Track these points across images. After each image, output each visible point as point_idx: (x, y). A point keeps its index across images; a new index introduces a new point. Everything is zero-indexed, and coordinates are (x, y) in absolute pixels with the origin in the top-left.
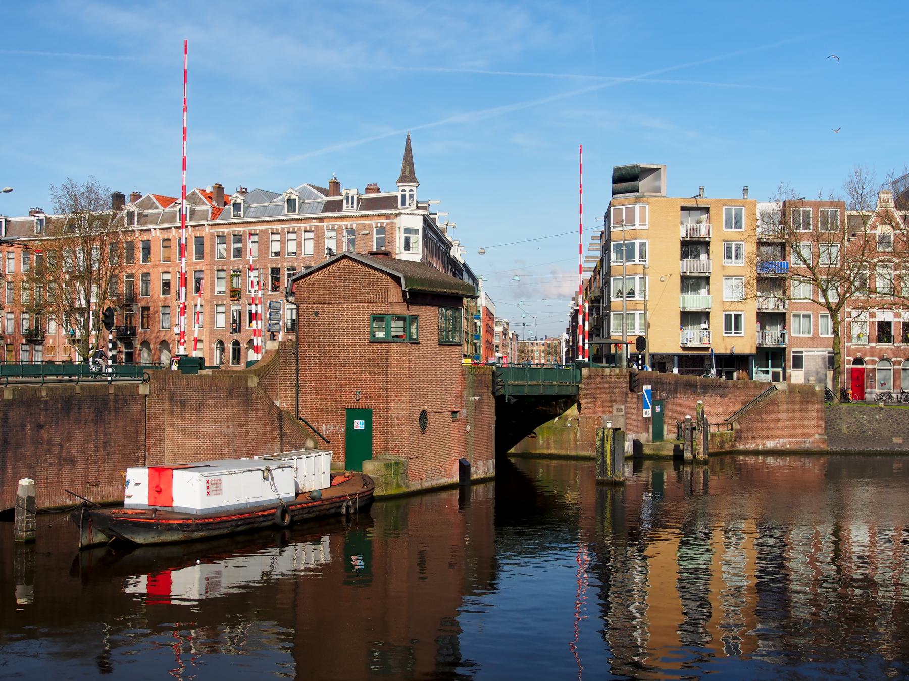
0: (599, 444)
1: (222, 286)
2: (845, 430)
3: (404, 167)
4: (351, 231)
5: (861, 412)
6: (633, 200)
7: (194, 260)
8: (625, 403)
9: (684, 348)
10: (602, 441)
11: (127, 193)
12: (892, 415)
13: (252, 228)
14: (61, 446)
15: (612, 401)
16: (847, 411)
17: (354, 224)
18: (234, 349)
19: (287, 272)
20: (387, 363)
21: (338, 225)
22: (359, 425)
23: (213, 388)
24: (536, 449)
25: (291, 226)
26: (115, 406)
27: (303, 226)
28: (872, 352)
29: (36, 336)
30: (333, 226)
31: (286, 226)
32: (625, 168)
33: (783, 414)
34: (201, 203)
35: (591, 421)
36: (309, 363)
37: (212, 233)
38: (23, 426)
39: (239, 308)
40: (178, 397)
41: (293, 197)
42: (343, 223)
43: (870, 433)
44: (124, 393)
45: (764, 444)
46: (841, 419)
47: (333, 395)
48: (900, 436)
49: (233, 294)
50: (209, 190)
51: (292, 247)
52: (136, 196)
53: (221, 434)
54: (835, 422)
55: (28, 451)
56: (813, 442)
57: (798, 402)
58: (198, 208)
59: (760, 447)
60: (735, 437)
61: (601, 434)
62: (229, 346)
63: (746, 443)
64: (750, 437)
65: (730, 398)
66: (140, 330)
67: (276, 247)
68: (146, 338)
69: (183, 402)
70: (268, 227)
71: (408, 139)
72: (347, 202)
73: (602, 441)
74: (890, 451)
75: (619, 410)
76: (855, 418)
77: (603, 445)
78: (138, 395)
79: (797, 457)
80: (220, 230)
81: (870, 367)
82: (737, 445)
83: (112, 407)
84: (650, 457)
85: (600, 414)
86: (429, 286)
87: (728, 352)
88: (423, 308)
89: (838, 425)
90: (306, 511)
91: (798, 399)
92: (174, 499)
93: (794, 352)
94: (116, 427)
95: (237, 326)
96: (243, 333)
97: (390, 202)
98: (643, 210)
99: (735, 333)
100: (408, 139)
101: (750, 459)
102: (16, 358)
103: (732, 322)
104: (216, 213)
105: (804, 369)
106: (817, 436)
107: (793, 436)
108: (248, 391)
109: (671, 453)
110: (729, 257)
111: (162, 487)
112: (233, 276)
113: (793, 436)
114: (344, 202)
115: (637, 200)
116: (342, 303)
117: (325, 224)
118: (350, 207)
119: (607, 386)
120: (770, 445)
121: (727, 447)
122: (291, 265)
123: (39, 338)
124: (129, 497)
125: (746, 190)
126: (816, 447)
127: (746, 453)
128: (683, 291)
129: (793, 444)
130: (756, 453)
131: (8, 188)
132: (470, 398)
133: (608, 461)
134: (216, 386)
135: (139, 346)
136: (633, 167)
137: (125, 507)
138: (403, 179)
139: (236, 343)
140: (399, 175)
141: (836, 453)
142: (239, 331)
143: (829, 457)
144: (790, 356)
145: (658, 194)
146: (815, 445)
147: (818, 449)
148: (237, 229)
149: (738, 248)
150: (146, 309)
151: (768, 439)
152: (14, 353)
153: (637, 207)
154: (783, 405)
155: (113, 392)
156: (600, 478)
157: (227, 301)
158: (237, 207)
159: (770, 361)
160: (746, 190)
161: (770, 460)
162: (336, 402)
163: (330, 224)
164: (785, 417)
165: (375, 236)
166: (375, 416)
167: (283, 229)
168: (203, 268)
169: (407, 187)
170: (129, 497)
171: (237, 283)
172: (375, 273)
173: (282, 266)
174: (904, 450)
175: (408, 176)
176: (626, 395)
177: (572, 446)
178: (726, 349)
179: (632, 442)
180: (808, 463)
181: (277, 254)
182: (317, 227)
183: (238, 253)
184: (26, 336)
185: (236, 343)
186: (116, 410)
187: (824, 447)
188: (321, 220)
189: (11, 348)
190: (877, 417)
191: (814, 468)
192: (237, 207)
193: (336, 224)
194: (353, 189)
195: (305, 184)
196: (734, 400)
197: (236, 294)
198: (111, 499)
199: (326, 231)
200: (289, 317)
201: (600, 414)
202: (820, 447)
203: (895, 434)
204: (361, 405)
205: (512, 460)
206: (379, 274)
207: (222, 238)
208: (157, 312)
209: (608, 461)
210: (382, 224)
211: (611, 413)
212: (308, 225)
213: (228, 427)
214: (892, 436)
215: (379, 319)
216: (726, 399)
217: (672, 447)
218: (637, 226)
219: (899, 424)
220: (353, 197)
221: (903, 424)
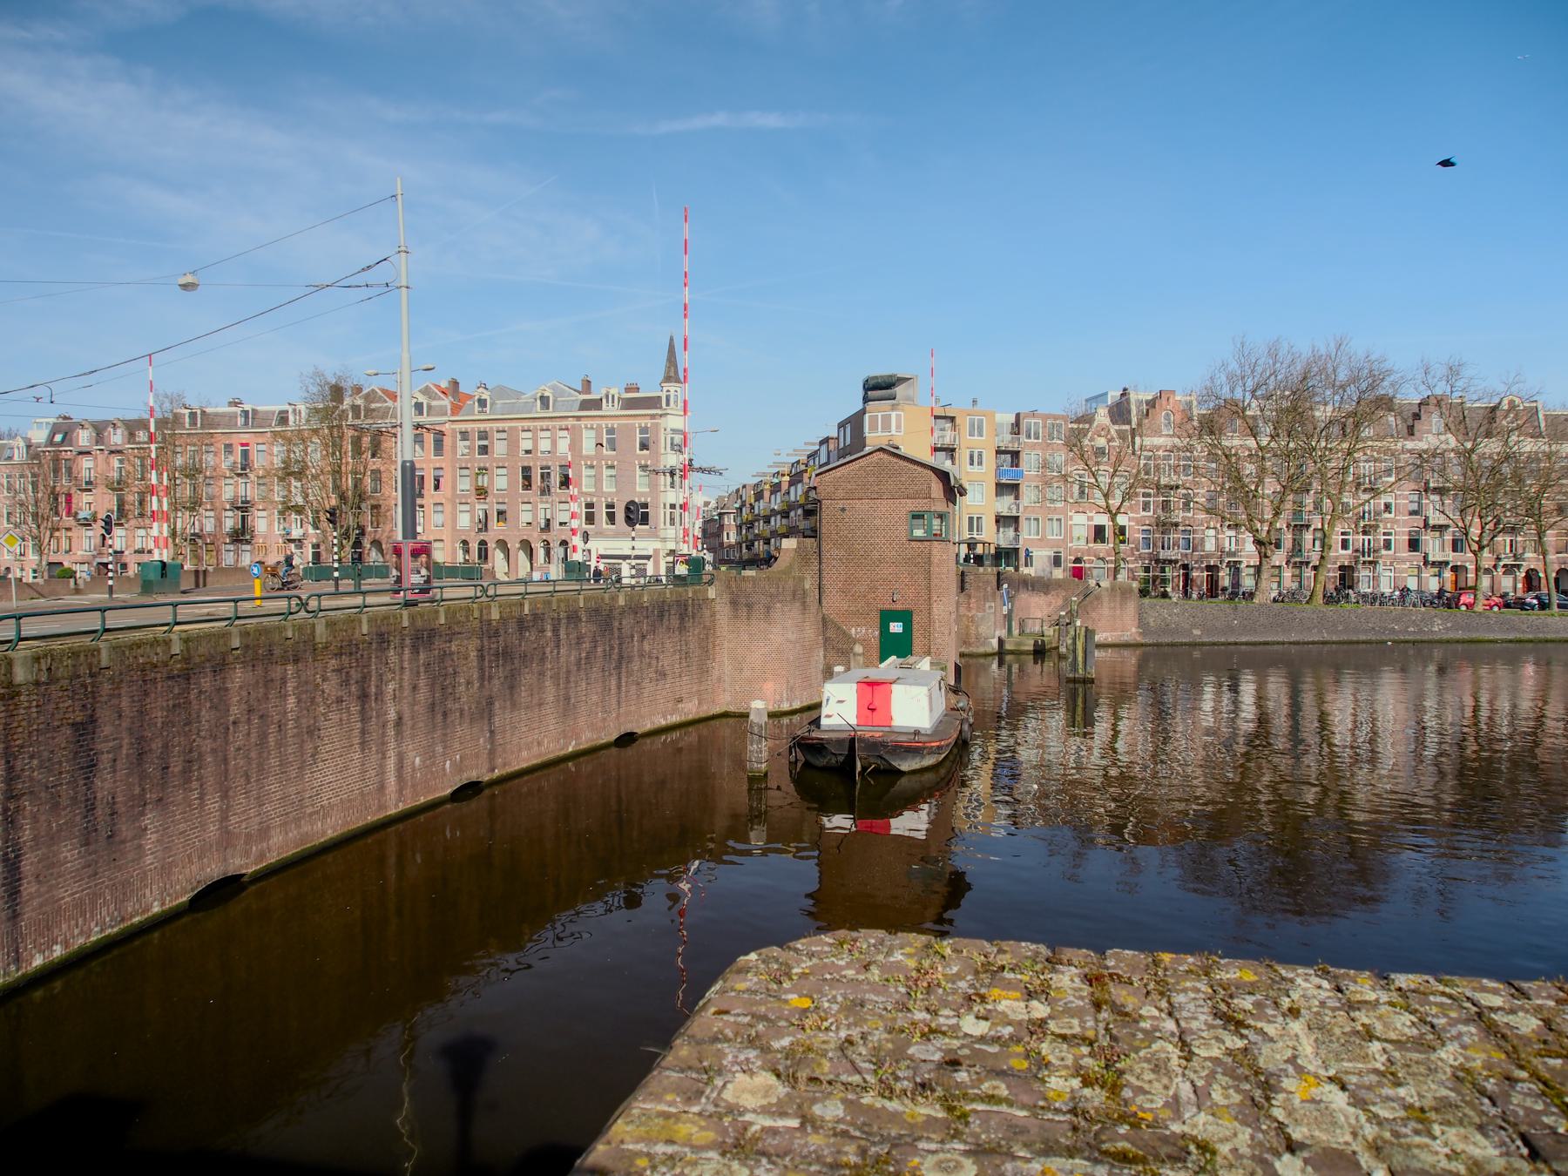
0: (1070, 642)
1: (465, 484)
2: (1152, 624)
4: (611, 431)
7: (433, 457)
10: (1074, 639)
11: (347, 385)
13: (500, 425)
14: (657, 658)
17: (616, 423)
18: (480, 550)
19: (540, 471)
20: (930, 563)
22: (896, 627)
25: (544, 424)
27: (558, 423)
28: (1089, 552)
29: (243, 534)
30: (592, 425)
31: (539, 424)
32: (881, 377)
34: (436, 398)
35: (964, 619)
36: (834, 563)
37: (454, 430)
38: (632, 637)
39: (486, 507)
40: (743, 600)
41: (546, 394)
42: (603, 423)
47: (865, 596)
49: (479, 492)
50: (444, 385)
51: (545, 445)
52: (358, 390)
55: (635, 666)
57: (1118, 599)
58: (434, 403)
61: (1072, 633)
62: (474, 546)
66: (370, 529)
67: (527, 445)
68: (377, 538)
69: (749, 606)
70: (519, 425)
71: (672, 339)
72: (607, 402)
73: (1074, 639)
75: (990, 607)
77: (1074, 643)
79: (1117, 649)
80: (463, 427)
81: (1087, 565)
84: (1012, 652)
92: (894, 717)
95: (484, 525)
97: (653, 402)
98: (898, 417)
104: (456, 409)
106: (1134, 630)
109: (1032, 648)
110: (972, 464)
111: (877, 704)
112: (478, 474)
114: (604, 401)
115: (894, 408)
117: (583, 423)
123: (248, 537)
124: (828, 716)
125: (975, 402)
128: (997, 496)
131: (431, 366)
133: (1080, 659)
135: (368, 546)
136: (891, 376)
137: (822, 728)
138: (668, 379)
139: (483, 543)
142: (486, 530)
143: (1143, 648)
144: (1022, 555)
148: (482, 426)
149: (980, 455)
150: (376, 507)
152: (214, 553)
153: (894, 414)
154: (1106, 599)
156: (1071, 675)
157: (472, 499)
158: (482, 403)
160: (975, 402)
162: (868, 604)
163: (589, 423)
165: (638, 436)
166: (916, 618)
167: (535, 427)
169: (672, 388)
170: (828, 716)
171: (484, 481)
172: (916, 467)
173: (535, 465)
175: (673, 374)
180: (1126, 653)
181: (528, 452)
182: (573, 426)
183: (484, 450)
184: (230, 535)
185: (483, 543)
187: (1140, 639)
188: (578, 418)
189: (210, 547)
191: (1131, 659)
192: (482, 403)
193: (595, 423)
194: (609, 387)
197: (482, 493)
198: (690, 717)
200: (543, 516)
203: (1194, 626)
204: (899, 606)
206: (919, 469)
207: (465, 435)
208: (388, 510)
209: (1080, 659)
211: (984, 611)
212: (564, 423)
215: (917, 516)
216: (1050, 596)
217: (1032, 642)
218: (893, 432)
220: (613, 396)
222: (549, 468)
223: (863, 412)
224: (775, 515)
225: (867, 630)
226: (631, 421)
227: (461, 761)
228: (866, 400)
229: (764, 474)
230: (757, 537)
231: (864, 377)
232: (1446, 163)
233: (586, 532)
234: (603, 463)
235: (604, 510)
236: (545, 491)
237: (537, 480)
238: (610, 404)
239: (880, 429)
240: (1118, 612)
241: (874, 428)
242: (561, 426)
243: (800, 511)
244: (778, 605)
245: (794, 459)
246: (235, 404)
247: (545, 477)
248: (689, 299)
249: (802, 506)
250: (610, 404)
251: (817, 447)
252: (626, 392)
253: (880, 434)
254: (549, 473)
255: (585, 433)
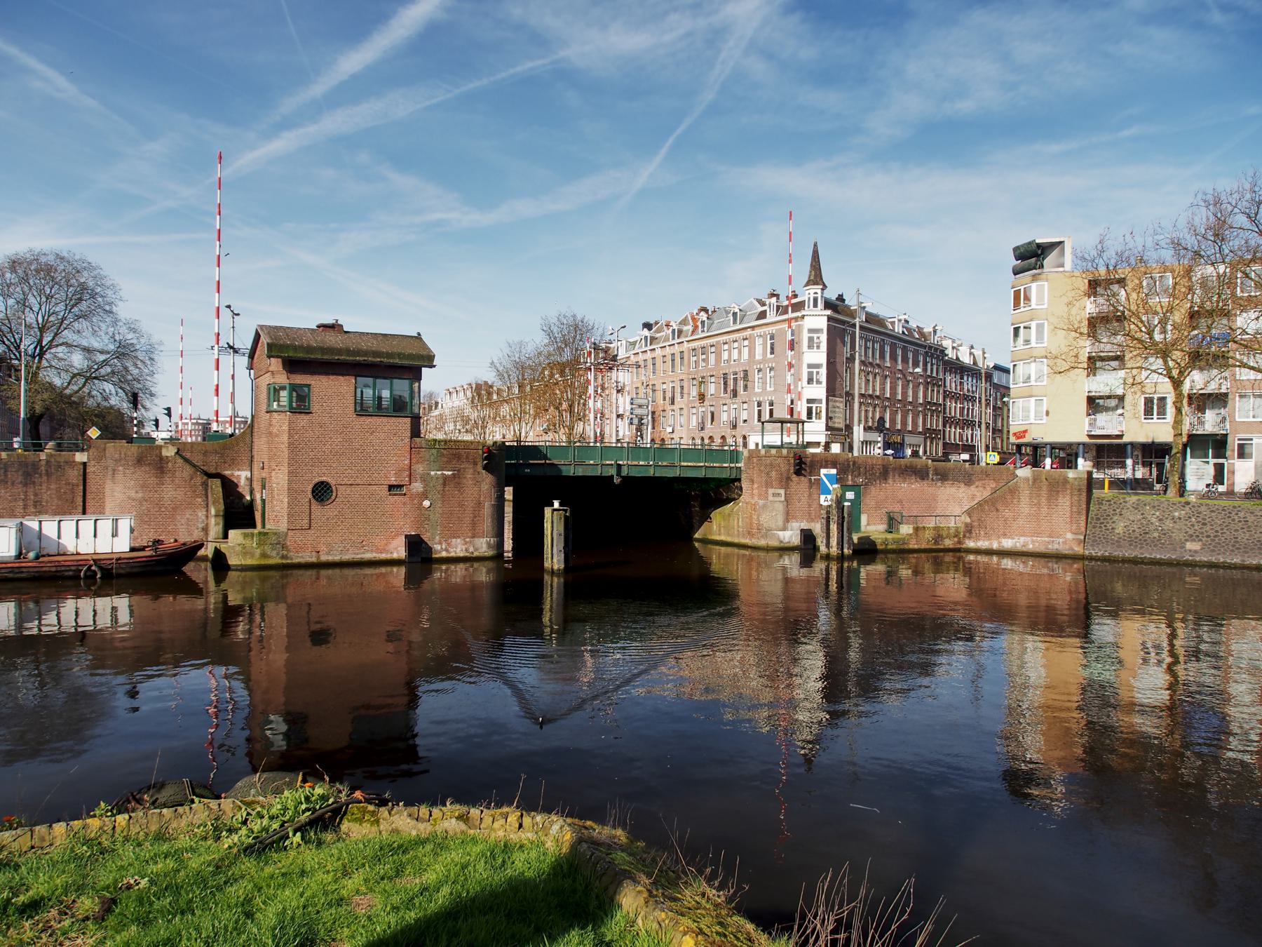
3: (811, 272)
5: (1154, 507)
6: (1030, 278)
8: (786, 488)
9: (1091, 437)
12: (1200, 513)
15: (768, 484)
16: (1134, 505)
23: (123, 456)
24: (711, 534)
26: (47, 471)
32: (1022, 246)
33: (1024, 505)
43: (1156, 535)
44: (58, 460)
45: (1000, 543)
46: (1121, 515)
48: (1201, 540)
51: (735, 355)
53: (129, 498)
54: (1111, 519)
56: (1065, 543)
57: (1044, 492)
59: (995, 546)
60: (964, 532)
63: (977, 539)
64: (982, 533)
65: (977, 487)
71: (815, 245)
74: (1175, 560)
76: (1142, 514)
78: (74, 462)
79: (1043, 560)
82: (967, 541)
83: (44, 472)
85: (756, 498)
86: (348, 355)
87: (1150, 440)
88: (316, 377)
89: (1114, 522)
90: (8, 570)
91: (1045, 488)
93: (1239, 440)
94: (48, 489)
96: (706, 431)
98: (1040, 290)
99: (1158, 419)
100: (815, 245)
101: (982, 559)
103: (1152, 407)
105: (1253, 460)
106: (1069, 536)
107: (1038, 534)
108: (162, 460)
112: (701, 382)
113: (1038, 534)
119: (762, 468)
120: (1008, 544)
121: (948, 543)
126: (1069, 550)
127: (977, 552)
129: (1037, 544)
130: (989, 552)
132: (433, 473)
134: (125, 454)
136: (1030, 243)
140: (806, 280)
141: (1091, 558)
144: (1233, 443)
145: (1061, 269)
146: (1067, 547)
147: (1071, 552)
151: (1005, 535)
153: (1034, 286)
155: (44, 458)
157: (697, 404)
159: (1210, 451)
161: (1007, 563)
164: (1027, 511)
174: (1198, 559)
176: (788, 479)
177: (736, 532)
178: (1148, 438)
179: (799, 532)
180: (1058, 568)
186: (48, 474)
187: (1078, 549)
188: (753, 328)
190: (1176, 514)
196: (981, 489)
197: (702, 397)
201: (756, 498)
202: (1073, 550)
203: (1191, 538)
205: (696, 544)
211: (767, 498)
213: (137, 492)
214: (1187, 540)
216: (972, 488)
218: (1033, 306)
219: (1206, 524)
221: (1212, 525)
240: (1044, 510)
244: (121, 468)
248: (215, 219)
253: (1022, 310)
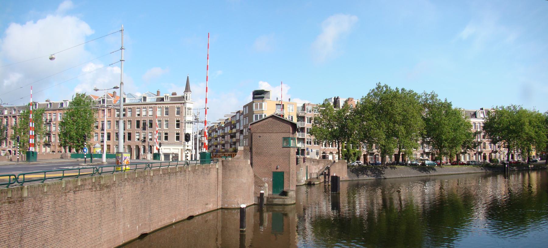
4: (167, 108)
17: (168, 106)
21: (162, 106)
42: (164, 105)
51: (144, 113)
102: (121, 169)
116: (271, 133)
117: (157, 105)
118: (167, 100)
122: (144, 119)
125: (289, 100)
160: (289, 100)
163: (159, 105)
168: (111, 120)
175: (187, 89)
181: (139, 115)
187: (348, 179)
188: (156, 104)
193: (161, 106)
195: (148, 92)
199: (158, 108)
210: (179, 106)
222: (145, 121)
223: (253, 102)
224: (219, 137)
225: (268, 179)
226: (174, 105)
227: (141, 226)
228: (254, 98)
229: (215, 123)
230: (219, 144)
231: (253, 90)
232: (51, 59)
233: (160, 143)
234: (164, 119)
235: (164, 135)
236: (144, 129)
237: (141, 125)
238: (167, 99)
239: (259, 108)
241: (256, 107)
242: (143, 107)
243: (229, 136)
245: (226, 118)
246: (47, 101)
247: (144, 124)
249: (230, 134)
250: (167, 99)
251: (236, 114)
252: (46, 102)
254: (146, 123)
255: (158, 110)
